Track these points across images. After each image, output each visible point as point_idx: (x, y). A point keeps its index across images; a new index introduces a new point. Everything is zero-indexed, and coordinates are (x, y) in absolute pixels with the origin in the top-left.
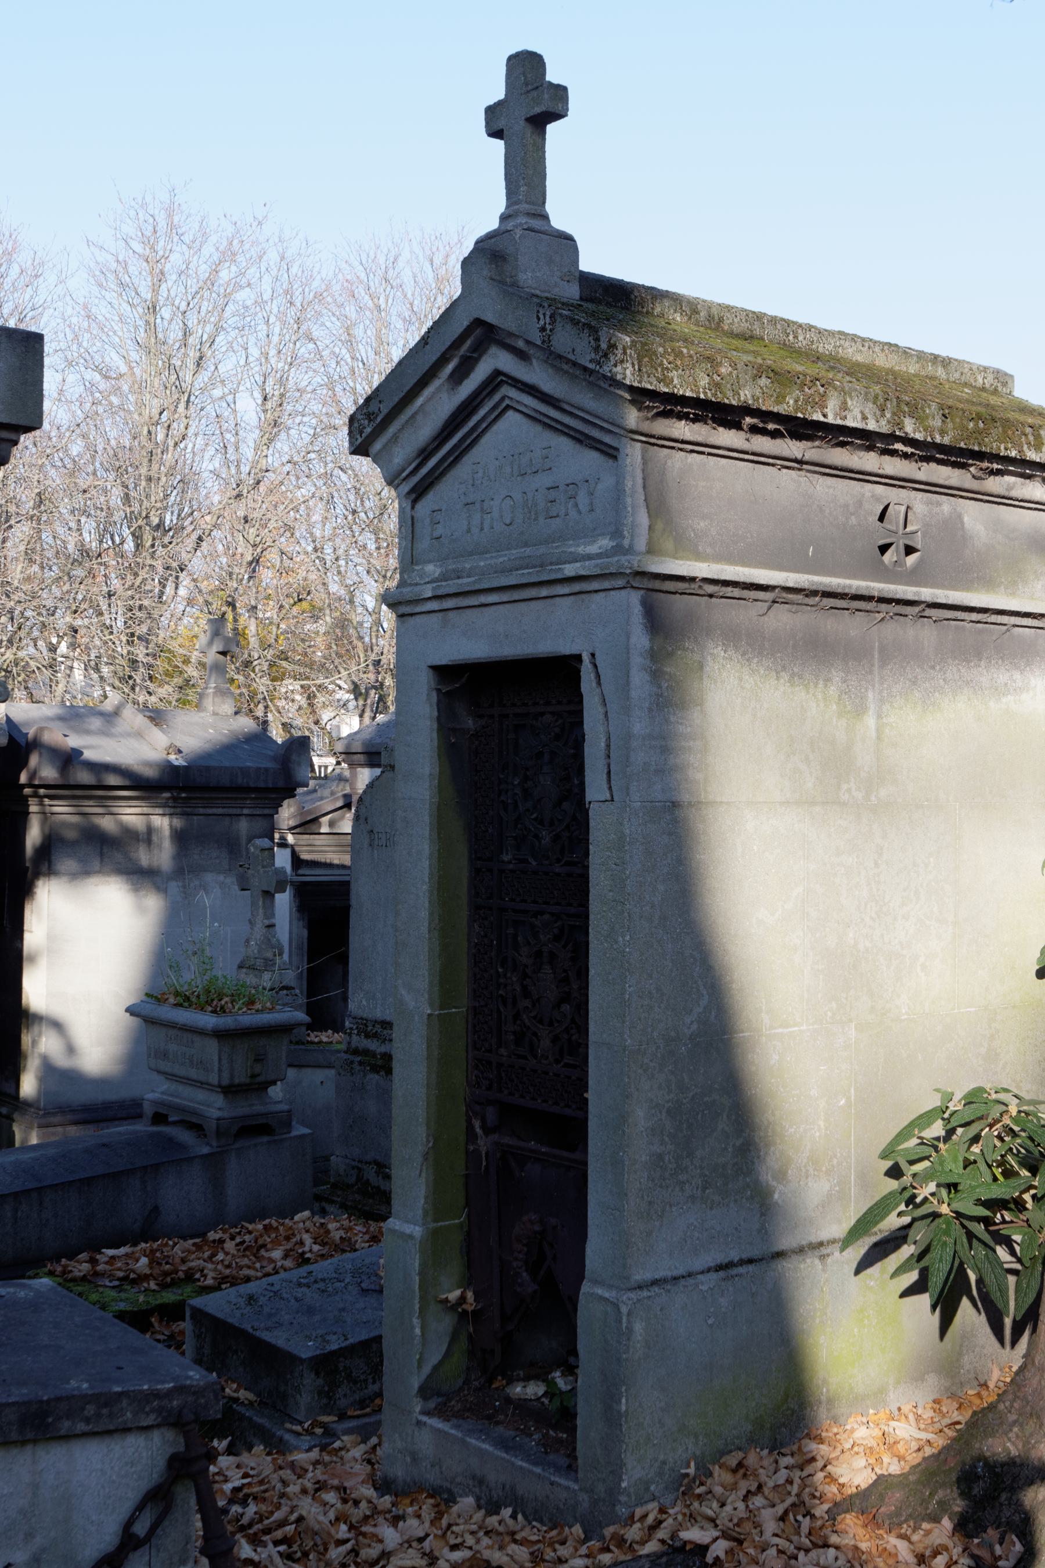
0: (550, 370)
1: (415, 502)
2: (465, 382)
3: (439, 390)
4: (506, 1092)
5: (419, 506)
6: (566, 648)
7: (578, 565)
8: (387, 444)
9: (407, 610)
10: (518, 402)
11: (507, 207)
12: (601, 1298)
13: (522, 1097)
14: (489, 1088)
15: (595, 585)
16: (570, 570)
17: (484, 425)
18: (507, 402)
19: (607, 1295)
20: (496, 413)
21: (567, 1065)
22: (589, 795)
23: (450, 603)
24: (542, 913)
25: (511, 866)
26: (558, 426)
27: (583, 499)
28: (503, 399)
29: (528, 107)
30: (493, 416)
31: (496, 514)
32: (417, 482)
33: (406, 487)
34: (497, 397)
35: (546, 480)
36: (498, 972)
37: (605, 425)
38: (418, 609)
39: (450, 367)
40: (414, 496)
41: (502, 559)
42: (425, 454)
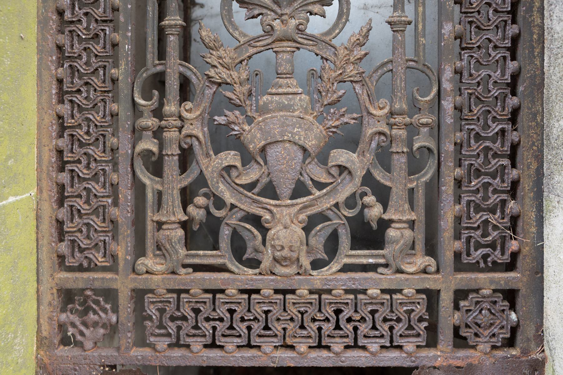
21: (346, 268)
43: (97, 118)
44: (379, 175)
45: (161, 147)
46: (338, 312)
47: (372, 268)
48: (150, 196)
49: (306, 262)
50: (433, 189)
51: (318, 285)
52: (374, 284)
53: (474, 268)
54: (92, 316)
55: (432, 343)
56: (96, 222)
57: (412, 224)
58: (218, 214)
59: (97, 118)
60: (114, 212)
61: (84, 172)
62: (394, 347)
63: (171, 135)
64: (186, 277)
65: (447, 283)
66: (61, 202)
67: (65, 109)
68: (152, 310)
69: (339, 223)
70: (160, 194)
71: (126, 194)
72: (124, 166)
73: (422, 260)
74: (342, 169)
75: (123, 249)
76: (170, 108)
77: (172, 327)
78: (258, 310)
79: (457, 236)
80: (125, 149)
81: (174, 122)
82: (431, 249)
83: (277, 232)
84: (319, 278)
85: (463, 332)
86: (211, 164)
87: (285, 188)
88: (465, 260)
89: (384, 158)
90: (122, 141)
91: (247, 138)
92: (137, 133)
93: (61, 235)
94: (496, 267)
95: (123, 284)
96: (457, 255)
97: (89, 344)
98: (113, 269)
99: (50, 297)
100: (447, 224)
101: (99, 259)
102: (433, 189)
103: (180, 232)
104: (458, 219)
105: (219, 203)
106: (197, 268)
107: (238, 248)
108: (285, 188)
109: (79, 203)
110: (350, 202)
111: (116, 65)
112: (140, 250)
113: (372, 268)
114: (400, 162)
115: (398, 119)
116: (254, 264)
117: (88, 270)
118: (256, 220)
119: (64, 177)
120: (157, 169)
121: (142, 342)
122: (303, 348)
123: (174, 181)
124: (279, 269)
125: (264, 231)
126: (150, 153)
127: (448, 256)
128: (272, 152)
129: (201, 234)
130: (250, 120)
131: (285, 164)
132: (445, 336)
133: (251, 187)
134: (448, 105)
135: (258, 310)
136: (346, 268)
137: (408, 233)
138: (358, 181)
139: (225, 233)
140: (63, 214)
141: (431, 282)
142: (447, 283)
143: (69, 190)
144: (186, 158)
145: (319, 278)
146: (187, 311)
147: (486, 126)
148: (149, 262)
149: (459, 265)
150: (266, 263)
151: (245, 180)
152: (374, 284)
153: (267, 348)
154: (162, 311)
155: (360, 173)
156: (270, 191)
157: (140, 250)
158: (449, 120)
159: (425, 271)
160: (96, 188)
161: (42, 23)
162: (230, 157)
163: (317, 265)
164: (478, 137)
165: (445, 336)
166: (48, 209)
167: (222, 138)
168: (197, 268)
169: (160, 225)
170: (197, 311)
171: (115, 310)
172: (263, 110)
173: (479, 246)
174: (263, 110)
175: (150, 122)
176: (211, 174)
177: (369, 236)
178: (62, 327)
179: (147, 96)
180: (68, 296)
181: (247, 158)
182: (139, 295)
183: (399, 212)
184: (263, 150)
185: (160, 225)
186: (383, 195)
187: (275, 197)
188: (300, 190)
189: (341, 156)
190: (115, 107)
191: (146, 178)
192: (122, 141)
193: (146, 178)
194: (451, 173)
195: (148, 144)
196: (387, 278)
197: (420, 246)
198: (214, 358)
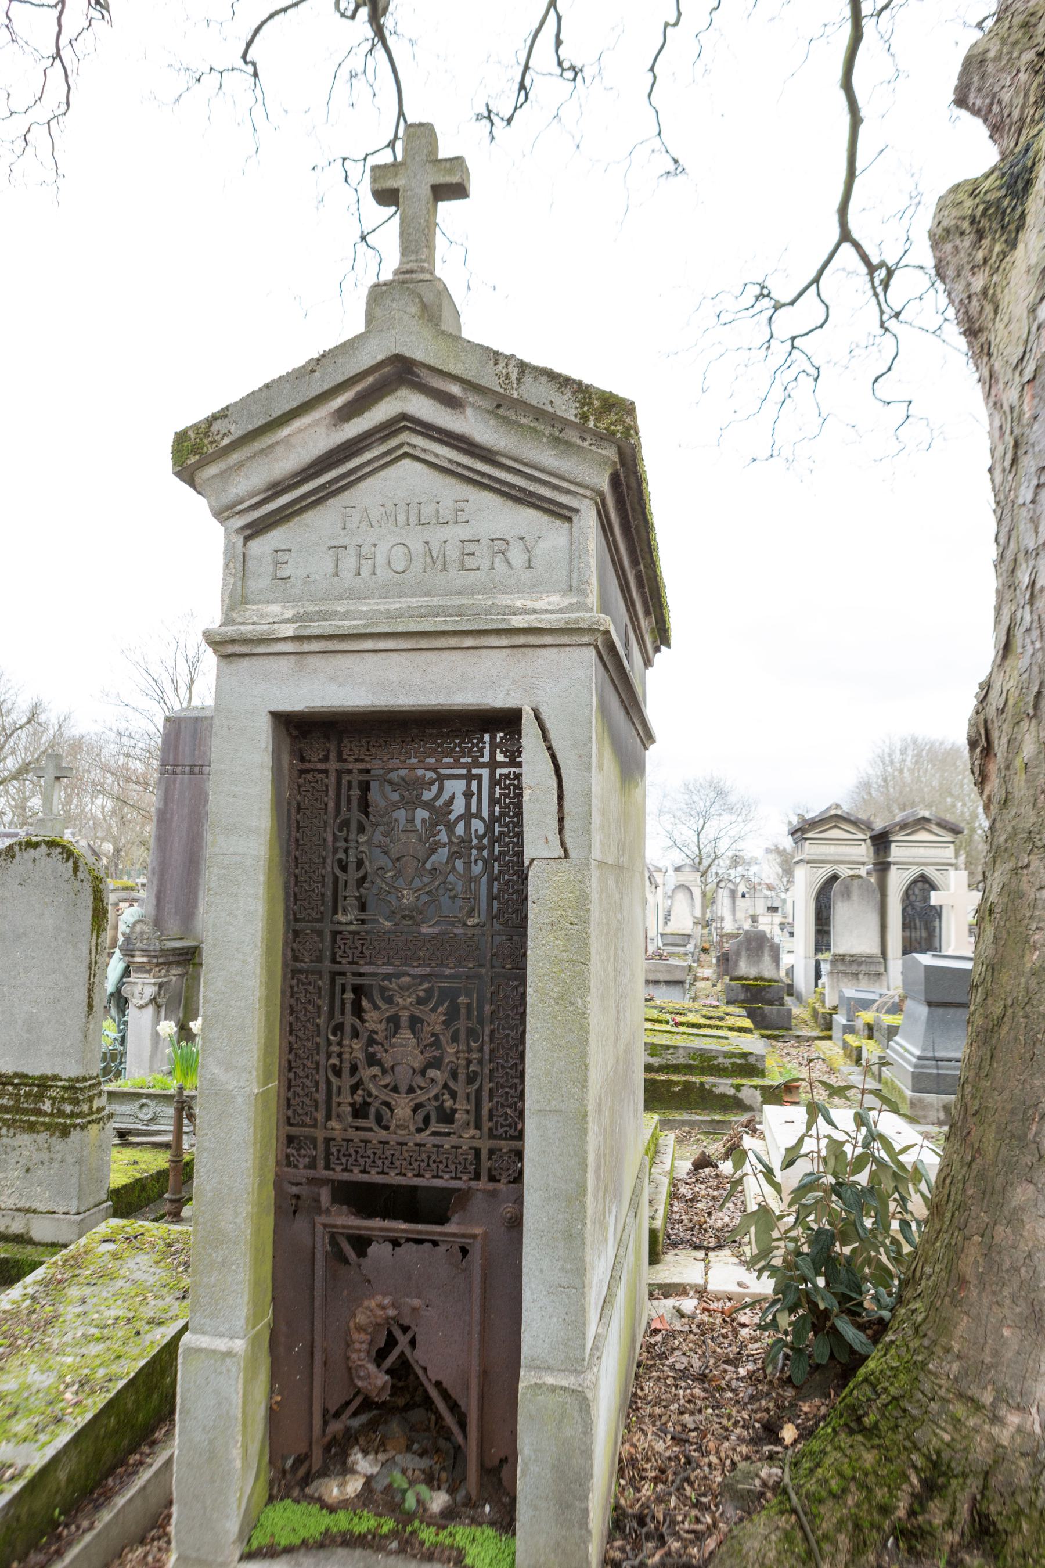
0: (492, 422)
1: (247, 539)
2: (355, 420)
3: (316, 423)
4: (339, 1168)
5: (253, 544)
6: (511, 703)
7: (532, 617)
8: (225, 471)
9: (230, 649)
10: (424, 450)
11: (401, 263)
12: (553, 1389)
13: (364, 1171)
14: (312, 1165)
15: (548, 640)
16: (518, 621)
17: (367, 469)
18: (406, 449)
19: (564, 1383)
20: (388, 459)
21: (434, 1134)
22: (530, 851)
23: (315, 646)
24: (398, 976)
25: (352, 928)
26: (486, 481)
27: (517, 556)
28: (401, 445)
29: (419, 181)
30: (382, 462)
31: (381, 559)
32: (259, 520)
33: (240, 522)
34: (393, 443)
35: (465, 532)
36: (328, 1039)
37: (565, 485)
38: (260, 650)
39: (339, 401)
40: (248, 532)
41: (396, 604)
42: (277, 489)
43: (309, 1045)
44: (451, 1084)
45: (341, 1062)
46: (429, 1157)
47: (448, 1134)
48: (335, 1089)
49: (412, 1128)
50: (479, 1091)
51: (418, 1141)
52: (447, 1143)
53: (500, 1137)
54: (303, 1152)
55: (477, 1177)
56: (307, 1101)
57: (468, 1112)
58: (369, 1100)
59: (309, 1045)
60: (317, 1096)
61: (301, 1074)
62: (456, 1178)
63: (346, 1056)
64: (351, 1133)
65: (485, 1145)
66: (289, 1088)
67: (292, 1039)
68: (334, 1150)
69: (431, 1107)
70: (339, 1088)
71: (323, 1086)
72: (322, 1071)
73: (472, 1132)
74: (432, 1080)
75: (320, 1116)
76: (346, 1042)
77: (344, 1160)
78: (388, 1153)
79: (490, 1119)
80: (323, 1062)
81: (347, 1049)
82: (478, 1127)
83: (399, 1112)
84: (419, 1138)
85: (494, 1173)
86: (366, 1073)
87: (403, 1088)
88: (339, 937)
89: (454, 1075)
90: (322, 1058)
91: (384, 1060)
92: (329, 1056)
93: (289, 1106)
94: (334, 954)
95: (320, 1134)
96: (490, 1129)
97: (301, 1166)
98: (315, 1126)
99: (283, 1139)
100: (485, 1112)
101: (308, 1120)
102: (479, 1091)
103: (349, 1109)
104: (491, 1111)
105: (370, 1095)
106: (357, 1129)
107: (379, 1119)
108: (403, 1088)
109: (299, 1090)
110: (436, 1097)
111: (319, 1017)
112: (328, 1117)
113: (448, 1134)
114: (462, 1077)
115: (461, 1055)
116: (387, 1128)
117: (302, 1126)
118: (387, 1104)
119: (291, 1075)
120: (338, 1072)
121: (327, 1167)
122: (410, 1175)
123: (347, 1081)
124: (400, 1132)
125: (392, 1111)
126: (334, 1065)
127: (485, 1130)
128: (396, 1069)
129: (360, 1111)
130: (386, 1051)
131: (403, 1076)
132: (484, 1176)
133: (386, 1086)
134: (487, 1049)
135: (388, 1153)
136: (434, 1134)
137: (465, 1116)
138: (440, 1087)
139: (373, 1110)
140: (290, 1095)
141: (476, 1144)
142: (485, 1145)
143: (293, 1083)
144: (354, 1069)
145: (419, 1138)
146: (351, 1151)
147: (507, 1061)
148: (333, 1124)
149: (492, 1136)
150: (392, 1128)
151: (383, 1083)
152: (447, 1143)
153: (392, 1174)
154: (339, 1151)
155: (441, 1083)
156: (395, 1089)
157: (328, 1117)
158: (487, 1057)
159: (473, 1137)
160: (308, 1082)
161: (283, 992)
162: (376, 1070)
163: (419, 1130)
164: (503, 1067)
165: (484, 1176)
166: (283, 1090)
167: (372, 1060)
168: (357, 1129)
169: (339, 1104)
170: (357, 1152)
171: (315, 1148)
172: (392, 1046)
173: (502, 1126)
174: (392, 1046)
175: (335, 1049)
176: (366, 1079)
177: (447, 1117)
178: (288, 1156)
179: (335, 1034)
180: (290, 1139)
181: (384, 1072)
182: (328, 1141)
183: (461, 1105)
184: (392, 1068)
185: (339, 1104)
186: (454, 1095)
187: (398, 1093)
188: (411, 1090)
189: (432, 1073)
190: (318, 1039)
191: (333, 1079)
192: (322, 1058)
193: (333, 1079)
194: (487, 1086)
195: (334, 1061)
196: (454, 1140)
197: (472, 1124)
198: (365, 1178)
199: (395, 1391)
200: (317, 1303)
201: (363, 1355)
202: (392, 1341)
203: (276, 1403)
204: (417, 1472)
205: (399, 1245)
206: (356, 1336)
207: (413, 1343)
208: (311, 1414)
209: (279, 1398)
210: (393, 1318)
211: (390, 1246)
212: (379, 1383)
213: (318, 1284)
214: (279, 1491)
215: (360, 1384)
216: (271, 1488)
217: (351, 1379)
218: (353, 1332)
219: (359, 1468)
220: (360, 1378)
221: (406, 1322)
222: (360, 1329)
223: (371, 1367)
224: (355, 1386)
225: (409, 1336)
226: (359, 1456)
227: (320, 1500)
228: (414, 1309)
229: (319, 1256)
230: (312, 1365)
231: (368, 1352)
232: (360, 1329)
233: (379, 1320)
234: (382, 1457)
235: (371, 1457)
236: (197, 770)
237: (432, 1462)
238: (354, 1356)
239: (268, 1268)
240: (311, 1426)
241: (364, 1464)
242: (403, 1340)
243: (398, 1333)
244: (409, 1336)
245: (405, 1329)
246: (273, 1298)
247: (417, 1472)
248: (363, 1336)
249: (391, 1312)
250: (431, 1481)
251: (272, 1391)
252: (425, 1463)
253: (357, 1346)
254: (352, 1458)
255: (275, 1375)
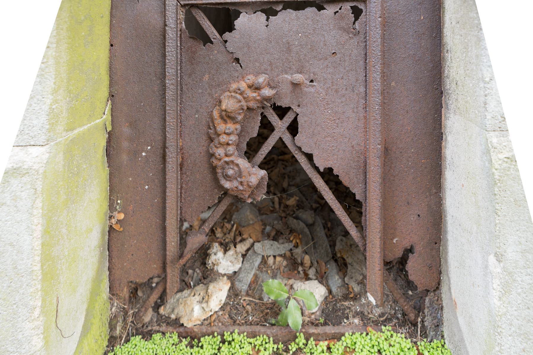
199: (273, 186)
200: (170, 94)
201: (231, 149)
202: (267, 127)
203: (119, 221)
204: (278, 259)
205: (275, 13)
206: (221, 127)
207: (293, 129)
208: (164, 229)
209: (122, 216)
210: (268, 99)
211: (263, 17)
212: (254, 180)
213: (170, 71)
214: (124, 328)
215: (227, 185)
216: (112, 327)
217: (216, 180)
218: (218, 121)
219: (221, 270)
220: (227, 177)
221: (283, 103)
222: (227, 117)
223: (243, 163)
224: (221, 187)
225: (289, 118)
226: (220, 254)
227: (177, 323)
228: (296, 85)
229: (171, 34)
230: (164, 171)
231: (238, 145)
232: (227, 117)
233: (252, 104)
234: (242, 248)
235: (231, 252)
236: (181, 244)
237: (291, 245)
238: (220, 152)
239: (99, 54)
240: (164, 242)
241: (224, 262)
242: (281, 126)
243: (273, 118)
244: (289, 118)
245: (281, 112)
246: (112, 96)
247: (278, 259)
248: (231, 127)
249: (267, 92)
250: (294, 268)
251: (112, 207)
252: (282, 248)
253: (224, 138)
254: (212, 259)
255: (113, 189)
